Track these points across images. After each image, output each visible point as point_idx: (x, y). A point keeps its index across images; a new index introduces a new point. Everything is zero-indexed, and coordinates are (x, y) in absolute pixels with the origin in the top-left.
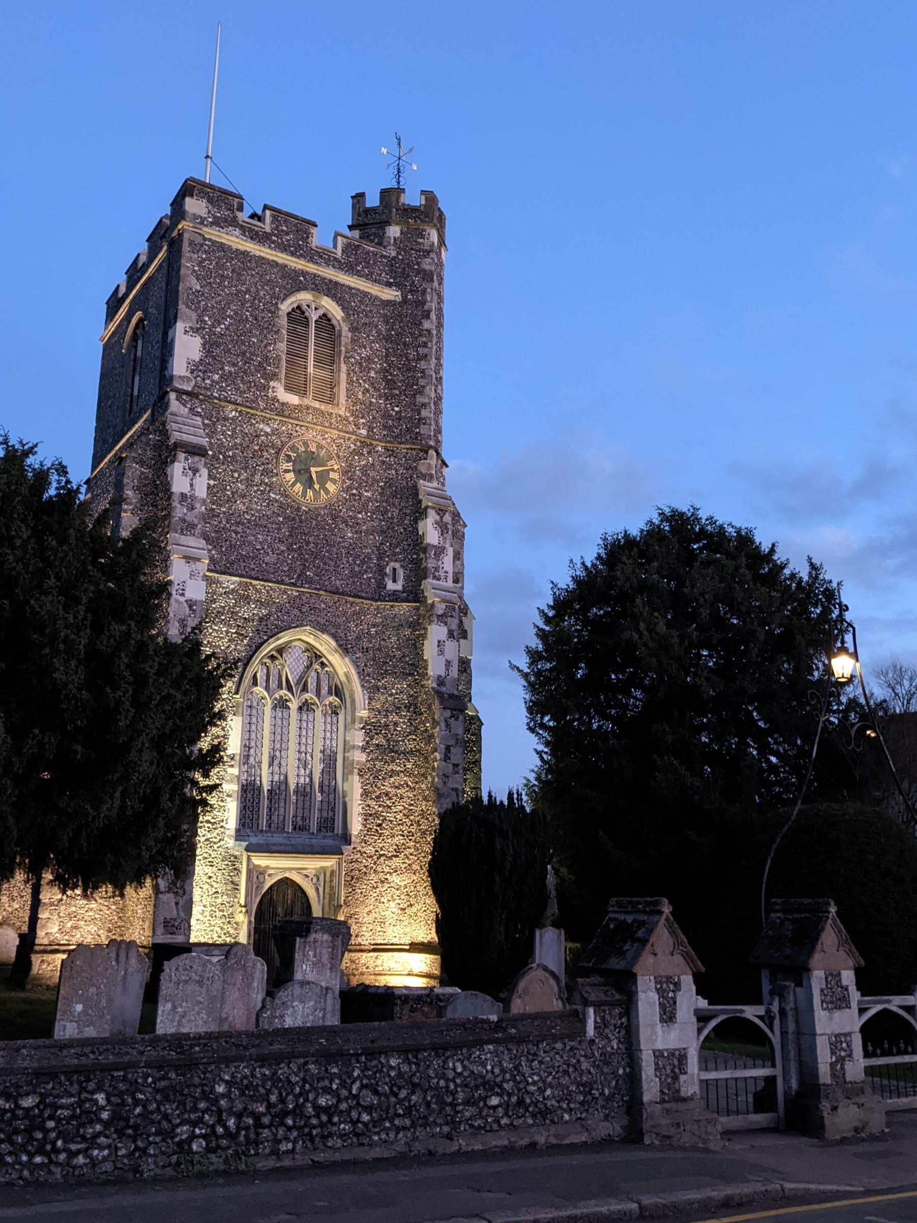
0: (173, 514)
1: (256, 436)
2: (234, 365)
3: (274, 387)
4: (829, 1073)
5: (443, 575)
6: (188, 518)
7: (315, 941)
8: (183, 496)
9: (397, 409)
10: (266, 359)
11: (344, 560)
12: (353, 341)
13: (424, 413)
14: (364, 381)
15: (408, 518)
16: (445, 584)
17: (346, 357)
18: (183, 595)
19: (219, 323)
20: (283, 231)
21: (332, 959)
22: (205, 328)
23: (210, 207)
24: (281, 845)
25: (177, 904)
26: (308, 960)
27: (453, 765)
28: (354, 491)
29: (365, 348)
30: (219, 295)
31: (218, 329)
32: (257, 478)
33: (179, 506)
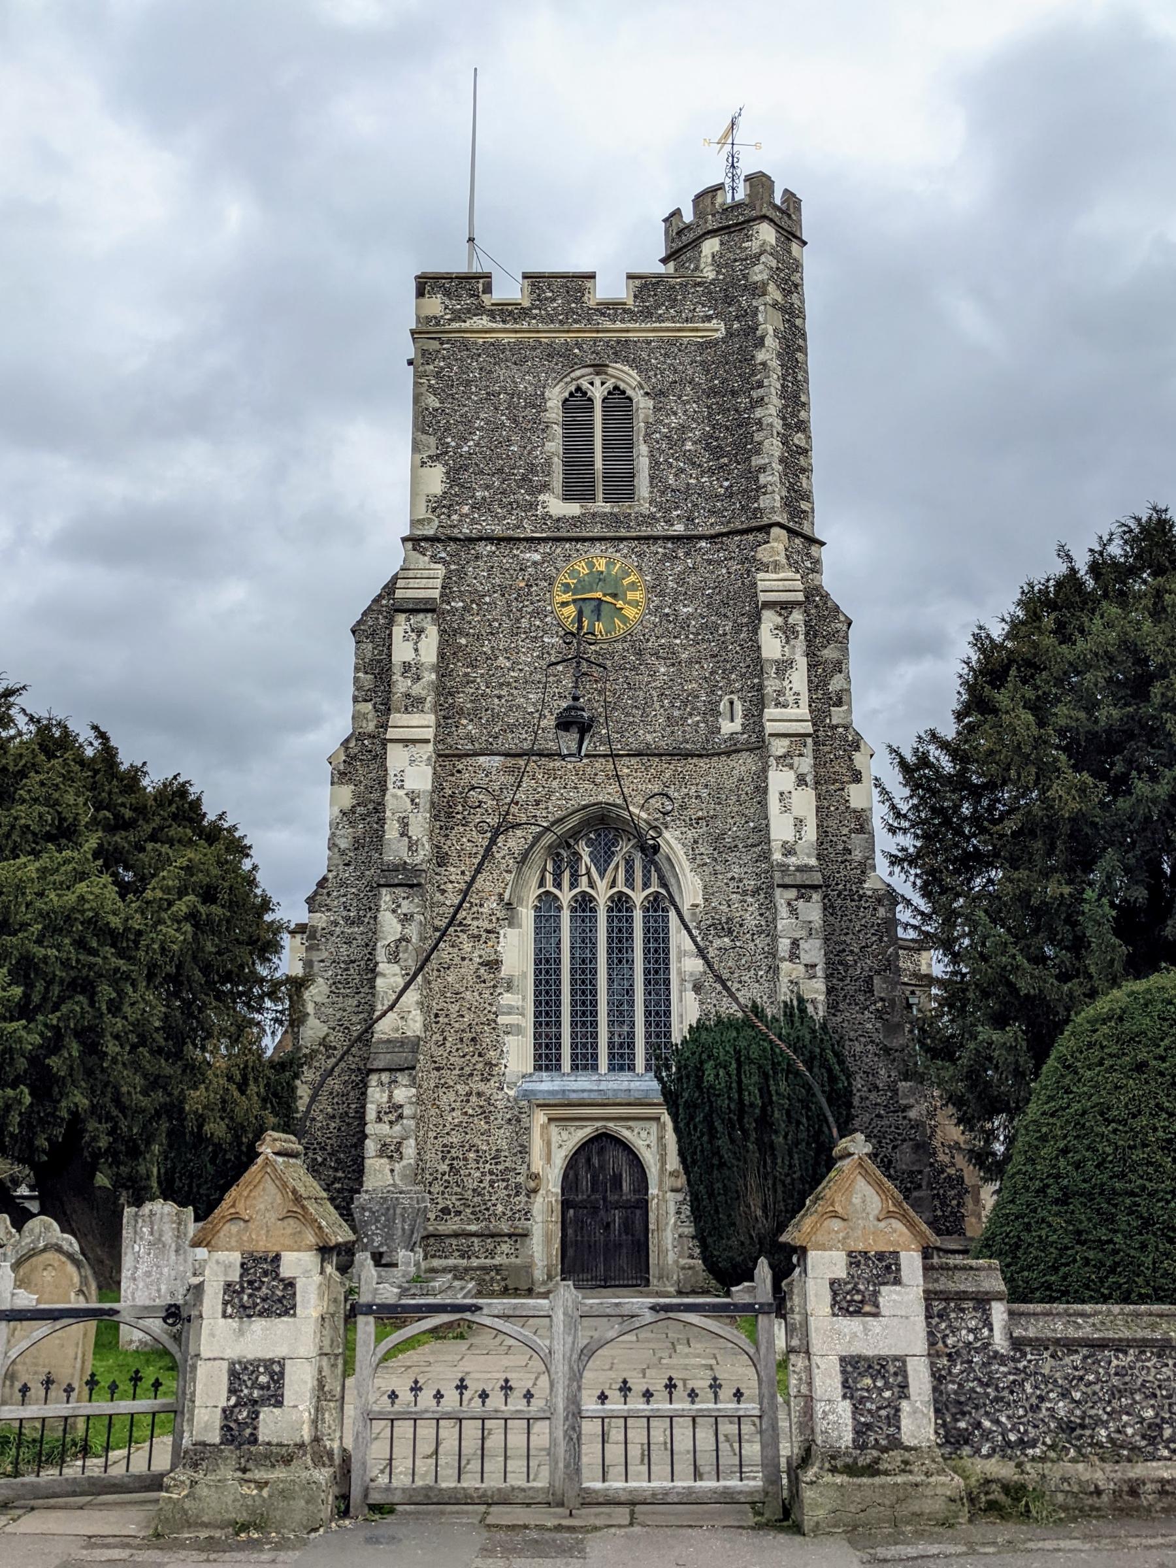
0: (394, 690)
1: (521, 569)
2: (487, 487)
3: (544, 502)
5: (791, 699)
6: (414, 693)
7: (152, 1214)
8: (407, 666)
9: (726, 484)
10: (532, 468)
11: (657, 705)
12: (657, 409)
13: (763, 479)
14: (677, 459)
15: (745, 629)
16: (797, 711)
17: (647, 435)
18: (402, 787)
19: (466, 440)
20: (546, 299)
21: (178, 1237)
22: (447, 453)
23: (447, 302)
24: (583, 1091)
25: (392, 1171)
26: (141, 1239)
27: (806, 965)
28: (667, 610)
29: (675, 414)
30: (464, 406)
31: (466, 449)
32: (524, 623)
33: (401, 679)
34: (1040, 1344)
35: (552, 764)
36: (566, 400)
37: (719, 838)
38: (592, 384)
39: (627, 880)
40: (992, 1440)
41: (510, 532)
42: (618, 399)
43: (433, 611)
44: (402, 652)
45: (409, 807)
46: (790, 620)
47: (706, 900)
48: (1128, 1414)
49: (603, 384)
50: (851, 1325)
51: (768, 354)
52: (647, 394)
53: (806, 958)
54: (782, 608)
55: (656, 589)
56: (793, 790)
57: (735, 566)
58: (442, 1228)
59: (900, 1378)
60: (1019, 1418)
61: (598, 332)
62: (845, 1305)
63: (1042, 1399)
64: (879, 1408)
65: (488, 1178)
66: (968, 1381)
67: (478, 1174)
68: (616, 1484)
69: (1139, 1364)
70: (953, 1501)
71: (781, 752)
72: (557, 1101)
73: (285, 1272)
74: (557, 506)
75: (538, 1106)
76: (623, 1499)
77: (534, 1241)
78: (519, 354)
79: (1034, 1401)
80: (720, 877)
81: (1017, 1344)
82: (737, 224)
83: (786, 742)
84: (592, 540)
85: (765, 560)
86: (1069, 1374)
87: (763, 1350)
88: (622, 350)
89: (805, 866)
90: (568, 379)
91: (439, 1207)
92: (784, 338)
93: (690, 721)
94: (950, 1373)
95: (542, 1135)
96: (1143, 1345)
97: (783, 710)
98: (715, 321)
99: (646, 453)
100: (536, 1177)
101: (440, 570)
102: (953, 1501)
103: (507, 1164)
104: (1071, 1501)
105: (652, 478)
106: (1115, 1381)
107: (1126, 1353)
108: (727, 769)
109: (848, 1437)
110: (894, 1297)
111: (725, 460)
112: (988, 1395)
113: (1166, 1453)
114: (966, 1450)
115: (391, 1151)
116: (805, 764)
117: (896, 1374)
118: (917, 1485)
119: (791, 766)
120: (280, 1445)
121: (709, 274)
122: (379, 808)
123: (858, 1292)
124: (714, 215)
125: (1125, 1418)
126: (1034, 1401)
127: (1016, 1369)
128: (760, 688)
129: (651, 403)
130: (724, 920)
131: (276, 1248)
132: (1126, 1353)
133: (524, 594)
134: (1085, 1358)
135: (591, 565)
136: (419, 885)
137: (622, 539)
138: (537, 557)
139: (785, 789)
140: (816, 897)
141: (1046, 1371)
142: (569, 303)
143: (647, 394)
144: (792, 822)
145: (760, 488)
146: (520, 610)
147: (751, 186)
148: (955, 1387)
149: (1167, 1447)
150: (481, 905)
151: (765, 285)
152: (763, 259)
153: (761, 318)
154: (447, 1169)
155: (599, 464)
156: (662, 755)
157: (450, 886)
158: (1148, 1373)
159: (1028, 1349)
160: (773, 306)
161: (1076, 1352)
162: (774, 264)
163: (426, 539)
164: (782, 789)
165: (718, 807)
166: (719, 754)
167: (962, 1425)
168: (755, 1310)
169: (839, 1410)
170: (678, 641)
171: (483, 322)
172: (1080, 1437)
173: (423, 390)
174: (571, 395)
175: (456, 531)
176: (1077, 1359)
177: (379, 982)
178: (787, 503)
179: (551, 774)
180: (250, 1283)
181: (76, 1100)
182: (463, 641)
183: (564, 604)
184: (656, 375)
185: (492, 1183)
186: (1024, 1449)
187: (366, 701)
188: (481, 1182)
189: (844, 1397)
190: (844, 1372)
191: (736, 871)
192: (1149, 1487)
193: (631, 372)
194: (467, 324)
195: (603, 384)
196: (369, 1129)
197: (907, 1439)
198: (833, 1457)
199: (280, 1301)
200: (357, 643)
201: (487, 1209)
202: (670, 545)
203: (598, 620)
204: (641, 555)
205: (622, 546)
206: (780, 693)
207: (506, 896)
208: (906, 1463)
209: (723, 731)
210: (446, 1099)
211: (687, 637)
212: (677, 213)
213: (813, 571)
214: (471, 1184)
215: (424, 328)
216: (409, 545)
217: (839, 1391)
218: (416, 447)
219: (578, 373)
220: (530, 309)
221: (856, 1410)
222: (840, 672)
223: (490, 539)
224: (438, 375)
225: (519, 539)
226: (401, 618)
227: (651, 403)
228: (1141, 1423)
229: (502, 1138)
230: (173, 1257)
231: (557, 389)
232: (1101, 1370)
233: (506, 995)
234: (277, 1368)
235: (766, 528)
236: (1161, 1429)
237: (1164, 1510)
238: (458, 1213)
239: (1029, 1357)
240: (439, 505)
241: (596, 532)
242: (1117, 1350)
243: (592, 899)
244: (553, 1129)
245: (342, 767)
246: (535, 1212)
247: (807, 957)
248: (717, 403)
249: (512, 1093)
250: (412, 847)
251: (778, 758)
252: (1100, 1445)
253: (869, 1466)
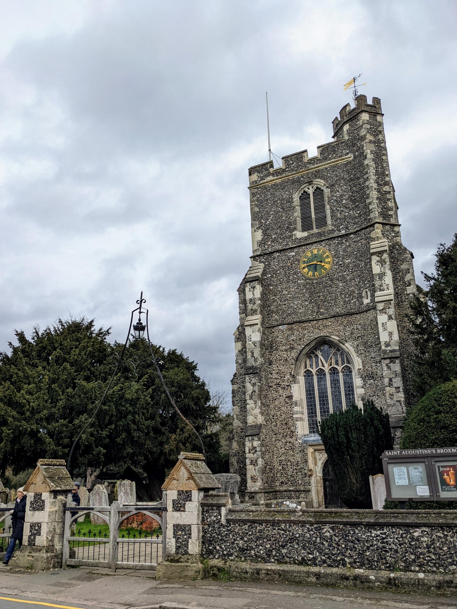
1: (289, 259)
2: (276, 234)
4: (27, 540)
5: (385, 287)
7: (124, 484)
8: (251, 300)
9: (358, 212)
10: (290, 224)
12: (331, 192)
13: (371, 207)
14: (340, 208)
17: (329, 201)
18: (251, 341)
20: (290, 164)
25: (255, 469)
28: (340, 263)
29: (338, 191)
31: (268, 222)
32: (291, 278)
34: (235, 521)
35: (304, 325)
36: (301, 197)
37: (366, 343)
38: (309, 189)
39: (336, 362)
40: (219, 553)
41: (284, 247)
42: (319, 192)
43: (257, 280)
44: (249, 295)
45: (253, 347)
46: (383, 258)
47: (363, 367)
48: (261, 546)
49: (312, 188)
50: (177, 514)
51: (369, 161)
52: (327, 187)
53: (395, 385)
54: (379, 254)
55: (336, 256)
56: (387, 322)
57: (363, 242)
58: (281, 489)
59: (189, 532)
60: (228, 546)
61: (308, 170)
62: (176, 508)
63: (235, 540)
64: (183, 541)
65: (295, 471)
66: (213, 533)
67: (292, 470)
68: (125, 563)
69: (266, 529)
70: (197, 572)
71: (381, 308)
72: (316, 444)
73: (43, 498)
74: (299, 234)
75: (309, 445)
76: (125, 567)
77: (313, 493)
78: (282, 186)
79: (233, 540)
80: (368, 357)
81: (228, 521)
82: (353, 117)
83: (383, 304)
84: (312, 243)
85: (374, 237)
86: (243, 532)
87: (163, 523)
88: (318, 174)
89: (394, 350)
90: (300, 189)
91: (280, 481)
92: (376, 153)
93: (352, 302)
94: (208, 531)
95: (312, 456)
96: (267, 522)
97: (383, 292)
98: (350, 154)
99: (329, 208)
100: (311, 470)
101: (262, 265)
102: (197, 572)
103: (301, 466)
104: (238, 575)
105: (332, 216)
106: (258, 534)
107: (262, 525)
108: (367, 317)
109: (174, 550)
110: (190, 505)
111: (357, 203)
112: (219, 538)
113: (273, 560)
114: (211, 556)
115: (254, 463)
116: (391, 311)
117: (188, 530)
118: (187, 566)
119: (385, 313)
120: (40, 546)
121: (346, 138)
123: (180, 504)
124: (346, 116)
125: (260, 547)
126: (233, 540)
127: (228, 529)
128: (374, 285)
129: (329, 190)
130: (370, 373)
131: (41, 492)
132: (262, 525)
133: (290, 268)
134: (249, 526)
135: (312, 252)
136: (257, 373)
137: (322, 241)
138: (293, 254)
139: (384, 322)
140: (397, 361)
141: (236, 531)
142: (298, 163)
143: (327, 187)
144: (388, 334)
145: (370, 211)
146: (289, 273)
147: (357, 101)
148: (209, 535)
149: (274, 558)
150: (285, 377)
151: (365, 135)
152: (364, 126)
153: (365, 149)
154: (281, 468)
155: (313, 216)
156: (342, 316)
157: (274, 371)
158: (269, 532)
159: (231, 523)
160: (370, 142)
161: (246, 524)
162: (369, 127)
163: (257, 256)
164: (383, 322)
165: (365, 332)
166: (363, 312)
167: (211, 548)
168: (161, 510)
169: (172, 541)
170: (345, 273)
171: (271, 178)
172: (246, 553)
173: (253, 206)
174: (302, 194)
175: (267, 251)
176: (246, 527)
177: (248, 406)
178: (381, 214)
179: (304, 329)
180: (35, 501)
181: (128, 451)
182: (272, 288)
183: (304, 268)
184: (330, 180)
185: (296, 473)
186: (229, 557)
187: (243, 313)
188: (293, 472)
189: (174, 537)
190: (174, 529)
191: (373, 355)
192: (263, 572)
193: (321, 181)
194: (265, 180)
195: (312, 188)
196: (247, 455)
197: (190, 552)
198: (169, 557)
199: (41, 506)
200: (239, 294)
201: (296, 482)
202: (340, 239)
203: (316, 271)
204: (329, 245)
205: (322, 243)
206: (381, 286)
207: (292, 373)
208: (188, 559)
209: (364, 303)
210: (279, 444)
211: (349, 271)
212: (336, 118)
213: (395, 236)
214: (290, 473)
215: (252, 186)
216: (252, 259)
217: (172, 535)
218: (252, 226)
219: (303, 186)
220: (285, 169)
221: (177, 542)
222: (409, 273)
223: (277, 251)
224: (257, 200)
225: (287, 249)
226: (248, 284)
227: (329, 190)
228: (266, 549)
229: (298, 457)
230: (130, 497)
231: (297, 194)
232: (254, 531)
233: (295, 407)
234: (39, 525)
235: (373, 225)
236: (272, 552)
237: (267, 580)
238: (286, 483)
239: (232, 526)
240: (262, 243)
241: (314, 240)
242: (259, 524)
243: (324, 371)
244: (317, 454)
245: (238, 336)
246: (312, 483)
247: (396, 384)
248: (353, 183)
249: (300, 441)
250: (256, 360)
251: (380, 311)
252: (252, 556)
253: (178, 559)
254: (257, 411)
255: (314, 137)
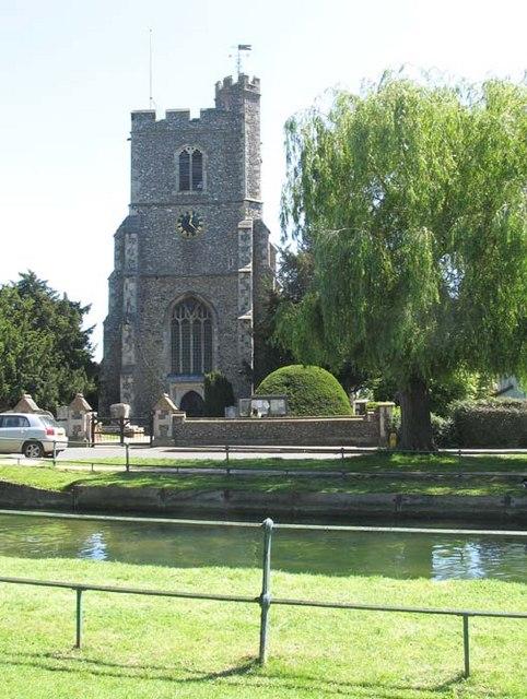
42: (197, 156)
122: (122, 295)
254: (132, 354)
255: (198, 100)
